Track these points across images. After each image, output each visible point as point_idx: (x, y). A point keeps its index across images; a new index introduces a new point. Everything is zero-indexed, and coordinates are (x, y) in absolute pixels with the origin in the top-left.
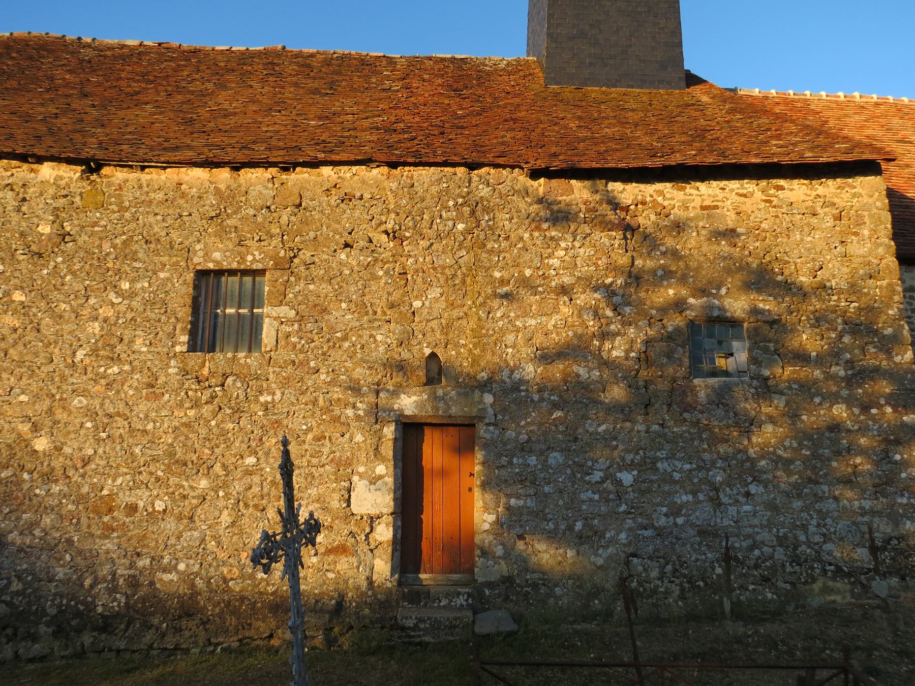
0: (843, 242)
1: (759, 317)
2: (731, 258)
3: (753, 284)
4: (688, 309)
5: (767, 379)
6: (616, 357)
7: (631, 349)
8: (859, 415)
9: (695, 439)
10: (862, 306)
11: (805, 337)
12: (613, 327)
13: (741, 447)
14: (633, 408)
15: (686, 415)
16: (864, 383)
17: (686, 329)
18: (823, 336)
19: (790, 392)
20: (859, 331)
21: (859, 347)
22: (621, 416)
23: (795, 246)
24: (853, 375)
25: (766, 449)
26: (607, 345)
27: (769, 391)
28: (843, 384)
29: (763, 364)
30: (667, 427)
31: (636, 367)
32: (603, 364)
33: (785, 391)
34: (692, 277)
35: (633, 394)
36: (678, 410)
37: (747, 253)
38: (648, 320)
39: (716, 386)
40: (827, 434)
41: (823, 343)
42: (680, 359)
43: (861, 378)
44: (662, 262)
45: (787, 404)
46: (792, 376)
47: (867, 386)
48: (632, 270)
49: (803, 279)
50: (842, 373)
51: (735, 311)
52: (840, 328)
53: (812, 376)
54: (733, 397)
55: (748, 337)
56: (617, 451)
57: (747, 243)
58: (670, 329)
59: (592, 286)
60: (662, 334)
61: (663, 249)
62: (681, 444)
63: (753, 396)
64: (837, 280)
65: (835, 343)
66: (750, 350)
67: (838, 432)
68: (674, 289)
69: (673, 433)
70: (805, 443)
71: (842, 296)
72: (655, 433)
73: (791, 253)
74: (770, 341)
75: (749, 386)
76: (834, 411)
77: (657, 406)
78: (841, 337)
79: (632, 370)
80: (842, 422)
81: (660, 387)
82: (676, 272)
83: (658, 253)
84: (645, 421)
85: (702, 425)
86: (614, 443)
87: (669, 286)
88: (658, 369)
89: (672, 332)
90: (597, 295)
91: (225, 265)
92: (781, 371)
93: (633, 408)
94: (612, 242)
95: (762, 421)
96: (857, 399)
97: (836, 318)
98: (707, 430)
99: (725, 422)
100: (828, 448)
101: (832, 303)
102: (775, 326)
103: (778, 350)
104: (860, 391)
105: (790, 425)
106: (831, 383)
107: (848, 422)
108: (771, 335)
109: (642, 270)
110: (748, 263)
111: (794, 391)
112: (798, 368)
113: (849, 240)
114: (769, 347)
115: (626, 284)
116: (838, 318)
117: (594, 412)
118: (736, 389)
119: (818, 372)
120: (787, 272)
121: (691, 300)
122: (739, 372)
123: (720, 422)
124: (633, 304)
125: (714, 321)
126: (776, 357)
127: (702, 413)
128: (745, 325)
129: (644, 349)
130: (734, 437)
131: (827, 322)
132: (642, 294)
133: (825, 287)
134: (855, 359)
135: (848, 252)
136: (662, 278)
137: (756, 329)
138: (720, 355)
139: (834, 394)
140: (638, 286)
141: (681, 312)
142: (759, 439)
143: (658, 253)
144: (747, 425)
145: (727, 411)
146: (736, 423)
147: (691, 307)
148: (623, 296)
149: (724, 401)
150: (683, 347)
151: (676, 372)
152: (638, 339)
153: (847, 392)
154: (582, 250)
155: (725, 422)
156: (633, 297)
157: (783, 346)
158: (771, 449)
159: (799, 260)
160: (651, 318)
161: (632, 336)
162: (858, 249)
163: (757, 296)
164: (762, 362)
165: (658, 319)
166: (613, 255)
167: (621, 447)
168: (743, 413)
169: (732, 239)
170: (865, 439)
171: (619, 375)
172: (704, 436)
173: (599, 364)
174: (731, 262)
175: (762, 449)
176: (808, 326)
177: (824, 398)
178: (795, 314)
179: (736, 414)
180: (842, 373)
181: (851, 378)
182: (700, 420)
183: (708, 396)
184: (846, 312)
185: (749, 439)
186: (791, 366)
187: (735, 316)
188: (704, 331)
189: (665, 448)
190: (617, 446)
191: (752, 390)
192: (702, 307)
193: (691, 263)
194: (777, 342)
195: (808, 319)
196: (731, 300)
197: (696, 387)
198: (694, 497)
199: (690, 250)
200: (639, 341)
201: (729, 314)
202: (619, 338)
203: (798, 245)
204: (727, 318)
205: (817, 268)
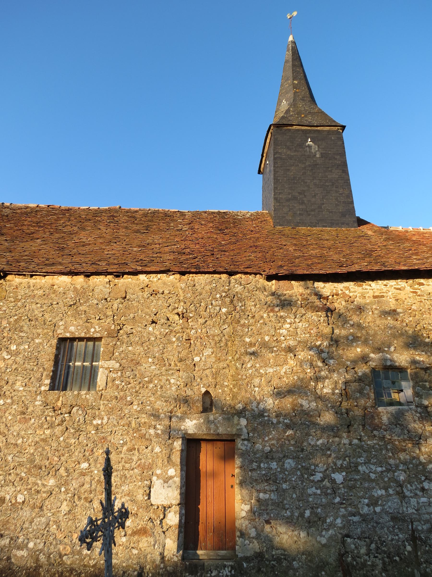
2: (395, 328)
3: (411, 344)
4: (370, 361)
6: (326, 393)
9: (383, 449)
12: (323, 373)
14: (340, 428)
15: (375, 432)
26: (320, 385)
29: (423, 397)
31: (340, 400)
34: (371, 340)
35: (339, 418)
37: (405, 324)
39: (394, 412)
42: (368, 394)
44: (351, 331)
48: (333, 336)
54: (405, 420)
55: (412, 379)
58: (360, 374)
60: (355, 377)
63: (419, 418)
66: (414, 387)
68: (360, 348)
69: (368, 445)
72: (356, 445)
74: (426, 381)
77: (355, 426)
79: (337, 402)
82: (361, 337)
83: (349, 325)
86: (329, 452)
87: (357, 346)
89: (361, 376)
94: (319, 319)
95: (427, 436)
102: (428, 371)
109: (339, 336)
110: (406, 331)
114: (425, 385)
117: (314, 430)
121: (372, 355)
122: (408, 402)
124: (335, 358)
125: (388, 369)
128: (409, 371)
129: (344, 387)
130: (409, 448)
136: (352, 341)
138: (394, 391)
140: (337, 346)
142: (427, 449)
145: (402, 429)
147: (372, 360)
149: (400, 422)
150: (369, 386)
152: (340, 381)
156: (335, 353)
160: (347, 367)
161: (336, 379)
165: (352, 367)
166: (320, 327)
167: (333, 455)
171: (329, 405)
172: (389, 447)
183: (389, 419)
185: (420, 449)
187: (401, 365)
189: (363, 456)
190: (331, 455)
193: (370, 331)
197: (380, 412)
199: (369, 323)
200: (340, 382)
201: (397, 364)
202: (327, 380)
204: (397, 366)
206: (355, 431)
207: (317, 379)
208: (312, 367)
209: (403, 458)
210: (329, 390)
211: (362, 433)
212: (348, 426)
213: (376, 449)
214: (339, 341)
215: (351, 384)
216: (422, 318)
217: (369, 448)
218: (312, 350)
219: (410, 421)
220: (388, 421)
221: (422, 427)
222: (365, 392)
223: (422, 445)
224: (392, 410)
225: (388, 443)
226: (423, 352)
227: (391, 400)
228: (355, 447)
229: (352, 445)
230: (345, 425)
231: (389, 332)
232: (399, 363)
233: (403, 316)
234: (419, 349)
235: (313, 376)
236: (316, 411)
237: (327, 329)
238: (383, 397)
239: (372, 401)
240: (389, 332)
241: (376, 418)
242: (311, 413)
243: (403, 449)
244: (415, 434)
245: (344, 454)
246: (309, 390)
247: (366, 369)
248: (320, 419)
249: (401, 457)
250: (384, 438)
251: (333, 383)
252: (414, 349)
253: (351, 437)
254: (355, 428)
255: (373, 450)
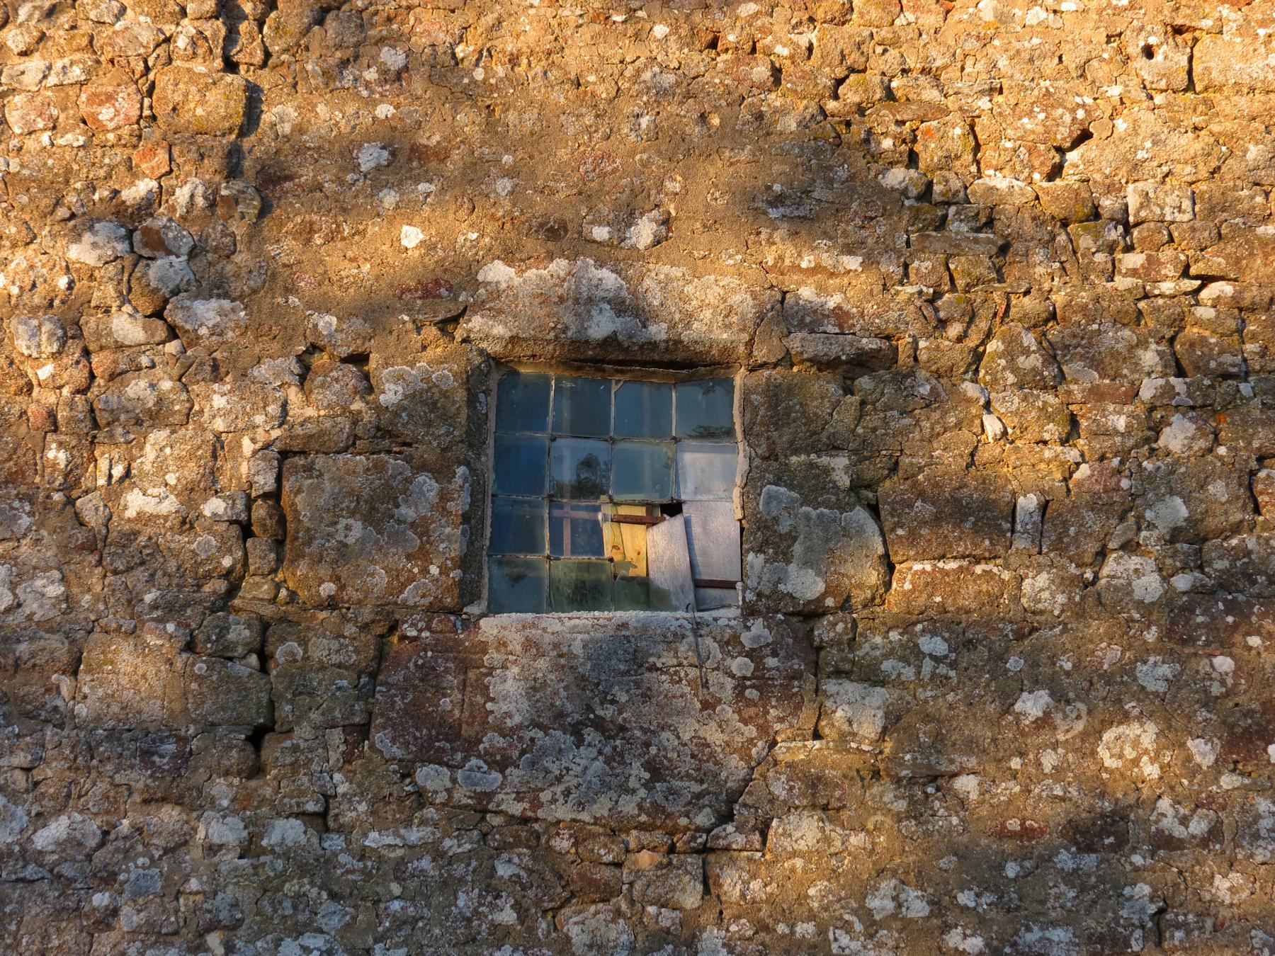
0: (1178, 30)
1: (796, 342)
2: (688, 95)
3: (777, 201)
4: (479, 306)
5: (812, 613)
6: (140, 515)
7: (210, 483)
8: (1217, 769)
9: (461, 881)
10: (1248, 297)
11: (992, 426)
12: (137, 388)
13: (667, 918)
14: (194, 744)
15: (431, 777)
16: (1244, 625)
17: (461, 395)
18: (1074, 421)
19: (908, 673)
20: (1233, 402)
21: (1229, 468)
22: (139, 779)
23: (971, 45)
24: (1195, 591)
25: (781, 928)
26: (103, 464)
27: (816, 669)
28: (1151, 636)
29: (798, 548)
30: (341, 830)
31: (227, 562)
32: (82, 548)
33: (886, 665)
34: (510, 173)
35: (200, 679)
36: (397, 751)
37: (761, 71)
38: (300, 358)
39: (577, 649)
40: (1065, 860)
41: (1072, 455)
42: (421, 528)
43: (1231, 607)
44: (384, 110)
45: (893, 721)
46: (922, 601)
47: (1254, 641)
48: (247, 143)
49: (1000, 181)
50: (1149, 585)
51: (689, 318)
52: (1148, 390)
53: (1016, 599)
54: (646, 696)
55: (746, 433)
56: (112, 937)
57: (766, 31)
58: (390, 394)
59: (62, 212)
60: (355, 419)
61: (393, 58)
62: (396, 906)
63: (740, 688)
64: (1149, 185)
65: (1124, 454)
66: (751, 483)
67: (1115, 848)
68: (425, 224)
69: (363, 854)
70: (965, 898)
71: (1167, 254)
72: (286, 855)
73: (953, 72)
74: (834, 448)
75: (724, 644)
76: (1102, 752)
77: (303, 733)
78: (1156, 430)
79: (208, 576)
80: (1139, 804)
81: (321, 649)
82: (441, 155)
83: (371, 75)
84: (241, 803)
85: (496, 821)
86: (101, 899)
87: (406, 211)
88: (324, 571)
89: (398, 410)
90: (82, 253)
91: (640, 529)
92: (873, 577)
93: (194, 744)
94: (169, 29)
95: (773, 799)
96: (1208, 702)
97: (1131, 348)
98: (518, 843)
99: (602, 808)
100: (1068, 919)
101: (1122, 283)
102: (865, 382)
103: (870, 486)
104: (1224, 663)
105: (899, 818)
106: (1097, 627)
107: (1164, 804)
108: (844, 418)
109: (295, 144)
110: (760, 116)
111: (928, 665)
112: (952, 565)
113: (1207, 23)
114: (827, 471)
115: (212, 205)
116: (1142, 344)
117: (21, 759)
118: (668, 659)
119: (1043, 579)
120: (929, 153)
121: (498, 272)
122: (699, 584)
123: (581, 805)
124: (237, 287)
125: (597, 363)
126: (860, 515)
127: (502, 764)
128: (740, 378)
129: (266, 481)
130: (638, 873)
131: (1096, 363)
132: (285, 249)
133: (1096, 214)
134: (1212, 523)
135: (1198, 68)
136: (379, 179)
137: (775, 395)
138: (624, 511)
139: (1108, 679)
140: (264, 211)
141: (447, 325)
142: (755, 885)
143: (371, 75)
144: (703, 818)
145: (615, 759)
146: (657, 809)
147: (492, 303)
148: (193, 254)
149: (608, 712)
150: (442, 472)
151: (400, 581)
152: (246, 442)
153: (1165, 670)
154: (35, 65)
155: (602, 808)
156: (238, 258)
157: (894, 468)
158: (805, 929)
159: (984, 103)
160: (314, 348)
161: (219, 424)
162: (1245, 57)
163: (789, 252)
164: (792, 537)
165: (344, 351)
166: (163, 80)
167: (129, 917)
168: (688, 766)
169: (697, 17)
170: (1236, 878)
171: (148, 598)
172: (504, 871)
173: (64, 549)
174: (689, 110)
175: (762, 927)
176: (1011, 378)
177: (1060, 697)
178: (955, 330)
179: (656, 771)
180: (1149, 585)
181: (1189, 609)
182: (489, 796)
183: (535, 688)
184: (1179, 322)
185: (708, 884)
186: (920, 557)
187: (686, 336)
188: (557, 408)
189: (320, 921)
190: (115, 912)
191: (740, 665)
192: (543, 298)
193: (512, 117)
194: (863, 451)
195: (1013, 350)
196: (676, 272)
197: (483, 648)
198: (884, 638)
199: (514, 60)
200: (247, 446)
201: (658, 331)
202: (158, 436)
203: (985, 41)
204: (653, 345)
205: (1063, 134)
206: (295, 766)
207: (96, 425)
208: (75, 351)
209: (586, 939)
210: (161, 499)
211: (338, 777)
212: (256, 738)
213: (413, 884)
214: (290, 178)
215: (320, 461)
216: (885, 33)
217: (367, 874)
218: (87, 237)
219: (680, 703)
220: (525, 705)
221: (751, 741)
222: (408, 512)
223: (733, 861)
224: (574, 630)
225: (503, 847)
226: (849, 250)
227: (599, 567)
228: (280, 864)
229: (264, 851)
230: (236, 723)
231: (644, 121)
232: (673, 326)
233: (756, 15)
234: (825, 235)
235: (71, 405)
236: (52, 631)
237: (213, 96)
238: (534, 547)
239: (444, 570)
240: (644, 121)
241: (452, 680)
242: (23, 648)
243: (592, 883)
244: (696, 788)
245: (196, 909)
246: (31, 499)
247: (440, 362)
248: (77, 689)
249: (574, 931)
250: (485, 811)
251: (191, 455)
252: (794, 234)
253: (263, 801)
254: (295, 748)
255: (396, 888)
